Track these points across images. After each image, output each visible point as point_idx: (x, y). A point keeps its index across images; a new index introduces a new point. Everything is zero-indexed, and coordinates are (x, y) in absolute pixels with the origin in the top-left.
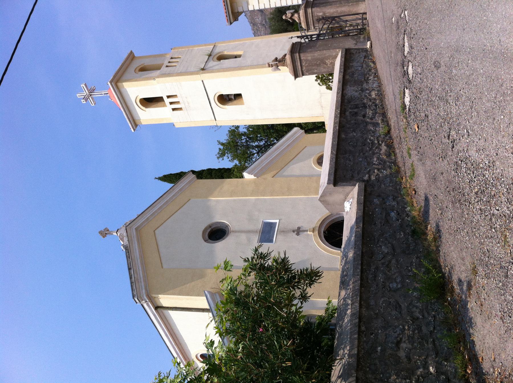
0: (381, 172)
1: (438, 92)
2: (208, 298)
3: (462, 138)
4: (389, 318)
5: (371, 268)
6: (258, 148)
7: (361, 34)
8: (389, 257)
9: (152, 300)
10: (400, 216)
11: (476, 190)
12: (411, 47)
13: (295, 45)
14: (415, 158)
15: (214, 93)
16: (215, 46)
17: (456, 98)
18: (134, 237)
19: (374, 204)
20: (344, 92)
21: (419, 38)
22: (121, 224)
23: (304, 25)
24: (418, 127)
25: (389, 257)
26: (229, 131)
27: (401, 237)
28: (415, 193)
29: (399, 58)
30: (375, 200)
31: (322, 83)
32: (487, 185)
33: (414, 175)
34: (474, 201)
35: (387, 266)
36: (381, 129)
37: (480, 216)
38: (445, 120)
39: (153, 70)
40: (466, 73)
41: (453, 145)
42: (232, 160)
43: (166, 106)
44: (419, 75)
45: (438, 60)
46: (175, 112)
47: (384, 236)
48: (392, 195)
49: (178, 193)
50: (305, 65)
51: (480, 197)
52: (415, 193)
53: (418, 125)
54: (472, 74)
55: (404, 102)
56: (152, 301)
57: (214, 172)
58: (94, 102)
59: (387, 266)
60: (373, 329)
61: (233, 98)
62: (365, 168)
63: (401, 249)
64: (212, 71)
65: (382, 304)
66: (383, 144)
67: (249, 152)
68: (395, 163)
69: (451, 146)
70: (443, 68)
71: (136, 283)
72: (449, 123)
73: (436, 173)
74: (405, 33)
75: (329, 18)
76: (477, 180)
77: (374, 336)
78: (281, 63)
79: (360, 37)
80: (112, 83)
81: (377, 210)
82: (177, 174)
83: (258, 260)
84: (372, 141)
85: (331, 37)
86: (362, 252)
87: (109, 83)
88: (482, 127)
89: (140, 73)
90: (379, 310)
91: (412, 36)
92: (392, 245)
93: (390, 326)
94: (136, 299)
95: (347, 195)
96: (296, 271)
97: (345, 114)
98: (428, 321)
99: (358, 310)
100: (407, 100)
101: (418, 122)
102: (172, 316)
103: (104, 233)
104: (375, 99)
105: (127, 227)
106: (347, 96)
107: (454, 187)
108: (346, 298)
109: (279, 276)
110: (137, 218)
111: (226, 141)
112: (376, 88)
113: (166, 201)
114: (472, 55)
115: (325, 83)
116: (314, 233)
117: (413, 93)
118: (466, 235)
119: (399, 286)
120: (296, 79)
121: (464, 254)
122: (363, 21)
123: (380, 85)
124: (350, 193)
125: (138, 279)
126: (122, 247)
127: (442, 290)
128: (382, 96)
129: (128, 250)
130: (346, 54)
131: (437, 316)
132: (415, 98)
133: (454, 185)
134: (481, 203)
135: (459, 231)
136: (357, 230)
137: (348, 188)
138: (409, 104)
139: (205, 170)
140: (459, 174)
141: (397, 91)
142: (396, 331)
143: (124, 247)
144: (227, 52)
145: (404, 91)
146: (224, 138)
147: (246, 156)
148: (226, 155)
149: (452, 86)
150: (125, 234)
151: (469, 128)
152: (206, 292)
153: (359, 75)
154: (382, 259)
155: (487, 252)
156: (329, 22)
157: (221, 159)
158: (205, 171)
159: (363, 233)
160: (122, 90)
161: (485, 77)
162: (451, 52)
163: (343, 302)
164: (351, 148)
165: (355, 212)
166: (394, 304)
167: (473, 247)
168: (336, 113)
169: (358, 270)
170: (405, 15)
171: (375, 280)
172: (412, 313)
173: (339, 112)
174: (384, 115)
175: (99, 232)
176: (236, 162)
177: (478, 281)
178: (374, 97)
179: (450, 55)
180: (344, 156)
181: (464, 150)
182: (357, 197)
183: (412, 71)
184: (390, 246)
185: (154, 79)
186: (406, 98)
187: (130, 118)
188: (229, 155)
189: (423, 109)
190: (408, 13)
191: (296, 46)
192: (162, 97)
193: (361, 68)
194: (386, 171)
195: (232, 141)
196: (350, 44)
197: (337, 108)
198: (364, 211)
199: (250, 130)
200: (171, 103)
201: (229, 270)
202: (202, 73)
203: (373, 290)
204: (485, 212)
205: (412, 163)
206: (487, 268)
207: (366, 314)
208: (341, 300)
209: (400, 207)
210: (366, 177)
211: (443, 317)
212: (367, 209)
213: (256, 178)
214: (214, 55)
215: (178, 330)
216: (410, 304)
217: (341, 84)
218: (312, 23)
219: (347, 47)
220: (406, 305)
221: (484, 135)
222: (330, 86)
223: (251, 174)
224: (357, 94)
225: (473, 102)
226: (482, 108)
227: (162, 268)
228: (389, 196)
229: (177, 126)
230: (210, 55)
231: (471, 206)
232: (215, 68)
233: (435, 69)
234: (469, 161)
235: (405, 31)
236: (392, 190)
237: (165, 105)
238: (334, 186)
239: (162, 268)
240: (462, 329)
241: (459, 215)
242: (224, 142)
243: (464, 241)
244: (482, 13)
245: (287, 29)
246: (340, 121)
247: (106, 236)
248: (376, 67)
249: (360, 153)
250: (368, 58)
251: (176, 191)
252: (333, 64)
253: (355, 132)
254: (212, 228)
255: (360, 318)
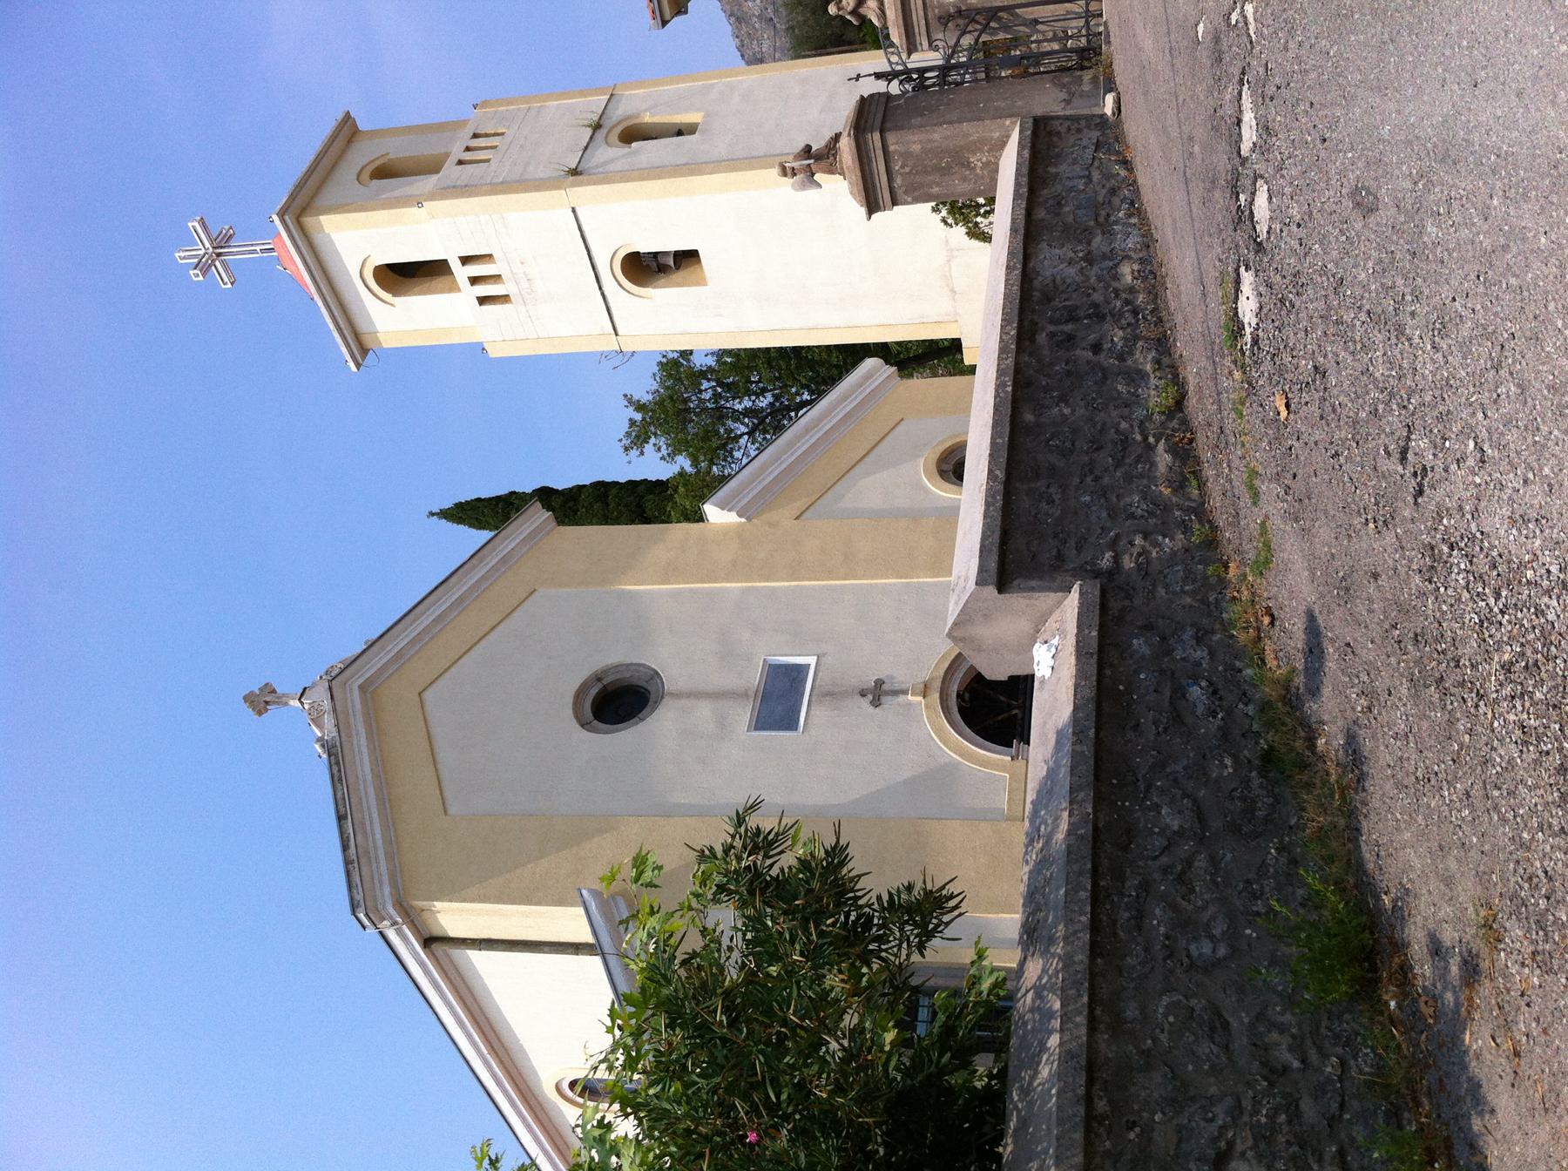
0: (1156, 544)
1: (1366, 295)
2: (591, 912)
3: (1454, 467)
4: (1190, 1067)
5: (1127, 886)
6: (753, 417)
7: (1082, 68)
8: (1187, 847)
9: (412, 918)
10: (1221, 699)
11: (1506, 657)
12: (1265, 128)
13: (870, 105)
14: (1273, 505)
15: (612, 242)
16: (612, 95)
17: (1438, 326)
18: (355, 715)
19: (1131, 656)
20: (1031, 265)
21: (1298, 99)
22: (314, 673)
23: (896, 35)
24: (1288, 406)
25: (1187, 847)
26: (660, 363)
27: (1225, 774)
28: (1272, 623)
29: (1222, 161)
30: (1135, 641)
31: (955, 219)
32: (1553, 648)
33: (1267, 562)
34: (1497, 691)
35: (1181, 879)
36: (1153, 392)
37: (1521, 751)
38: (1391, 395)
39: (420, 174)
40: (1481, 242)
41: (1420, 485)
42: (671, 456)
43: (459, 290)
44: (1294, 228)
45: (1370, 183)
46: (487, 308)
47: (1168, 770)
48: (1192, 625)
49: (498, 570)
50: (902, 171)
51: (1521, 684)
52: (1272, 623)
53: (1287, 398)
54: (1505, 248)
55: (1236, 314)
56: (412, 921)
57: (614, 491)
58: (229, 277)
59: (1181, 879)
60: (1136, 1107)
61: (671, 263)
62: (1102, 528)
63: (1226, 817)
64: (606, 178)
65: (1166, 1016)
66: (1161, 446)
67: (722, 431)
68: (1201, 511)
69: (1412, 490)
70: (1387, 214)
71: (363, 861)
72: (1404, 407)
73: (1352, 569)
74: (1242, 80)
75: (979, 11)
76: (1509, 622)
77: (1137, 1136)
78: (823, 164)
79: (1081, 76)
80: (287, 218)
81: (1142, 676)
82: (498, 498)
83: (745, 856)
84: (1123, 435)
85: (983, 75)
86: (1096, 828)
87: (275, 217)
88: (1537, 439)
89: (375, 182)
90: (1154, 1040)
91: (1271, 90)
92: (1195, 801)
93: (1193, 1099)
94: (362, 916)
95: (1044, 618)
96: (874, 900)
97: (1032, 340)
98: (1321, 1079)
99: (1085, 1039)
100: (1248, 308)
101: (1287, 388)
102: (474, 961)
103: (262, 701)
104: (1132, 290)
105: (334, 679)
106: (1040, 279)
107: (1419, 631)
108: (1044, 987)
109: (816, 930)
110: (364, 652)
111: (650, 397)
112: (1135, 251)
113: (457, 596)
114: (1506, 181)
115: (964, 220)
116: (928, 698)
117: (1269, 286)
118: (1461, 800)
119: (1222, 951)
120: (873, 216)
121: (1453, 865)
122: (1087, 23)
123: (1148, 242)
124: (1051, 614)
125: (367, 852)
126: (317, 747)
127: (1368, 971)
128: (1155, 278)
129: (336, 755)
130: (1035, 133)
131: (1352, 1062)
132: (1277, 304)
133: (1417, 624)
134: (1523, 706)
135: (1433, 782)
136: (1078, 748)
137: (1045, 600)
138: (1254, 322)
139: (585, 486)
140: (1442, 590)
141: (1212, 274)
142: (1214, 1116)
143: (323, 746)
144: (652, 115)
145: (1238, 275)
146: (646, 386)
147: (715, 443)
148: (653, 440)
149: (1420, 280)
150: (327, 704)
151: (1484, 434)
152: (585, 892)
153: (1078, 207)
154: (1162, 852)
155: (1545, 881)
156: (979, 27)
157: (634, 453)
158: (584, 490)
159: (1098, 758)
160: (318, 239)
161: (1557, 263)
162: (1420, 159)
163: (1033, 1001)
164: (1054, 459)
165: (1071, 683)
166: (1206, 1017)
167: (1487, 847)
168: (1004, 337)
169: (1084, 895)
170: (1245, 17)
171: (1139, 928)
172: (1266, 1050)
173: (1013, 332)
174: (1163, 345)
175: (246, 699)
176: (683, 463)
177: (1503, 967)
178: (1129, 281)
179: (1415, 172)
180: (1032, 485)
181: (1461, 508)
182: (1075, 631)
183: (1268, 213)
184: (1190, 805)
185: (419, 204)
186: (1242, 299)
187: (342, 326)
188: (662, 442)
189: (1305, 346)
190: (1255, 12)
191: (873, 107)
192: (445, 261)
193: (1086, 184)
194: (1172, 539)
195: (671, 398)
196: (1048, 100)
197: (1006, 321)
198: (1099, 682)
199: (725, 362)
200: (474, 280)
201: (650, 885)
202: (573, 185)
203: (1134, 966)
204: (1539, 739)
205: (1263, 523)
206: (1541, 933)
207: (1110, 1056)
208: (1027, 991)
209: (1220, 668)
210: (1106, 561)
211: (1372, 1066)
212: (1108, 672)
213: (743, 520)
214: (611, 125)
215: (500, 1012)
216: (1260, 1017)
217: (1020, 237)
218: (923, 30)
219: (1039, 112)
220: (1246, 1020)
221: (1546, 471)
222: (979, 228)
223: (729, 510)
224: (1072, 272)
225: (1502, 346)
226: (1539, 372)
227: (446, 814)
228: (1183, 628)
229: (494, 352)
230: (597, 127)
231: (1482, 708)
232: (611, 167)
233: (1356, 215)
234: (1481, 549)
235: (1243, 73)
236: (1191, 606)
237: (454, 288)
238: (1000, 592)
239: (446, 814)
240: (1439, 1116)
241: (1437, 728)
242: (646, 398)
243: (1453, 819)
244: (1552, 29)
245: (843, 35)
246: (1017, 364)
247: (267, 710)
248: (1135, 181)
249: (1085, 475)
250: (1109, 149)
251: (491, 565)
252: (993, 168)
253: (1067, 403)
254: (605, 682)
255: (1091, 1069)
